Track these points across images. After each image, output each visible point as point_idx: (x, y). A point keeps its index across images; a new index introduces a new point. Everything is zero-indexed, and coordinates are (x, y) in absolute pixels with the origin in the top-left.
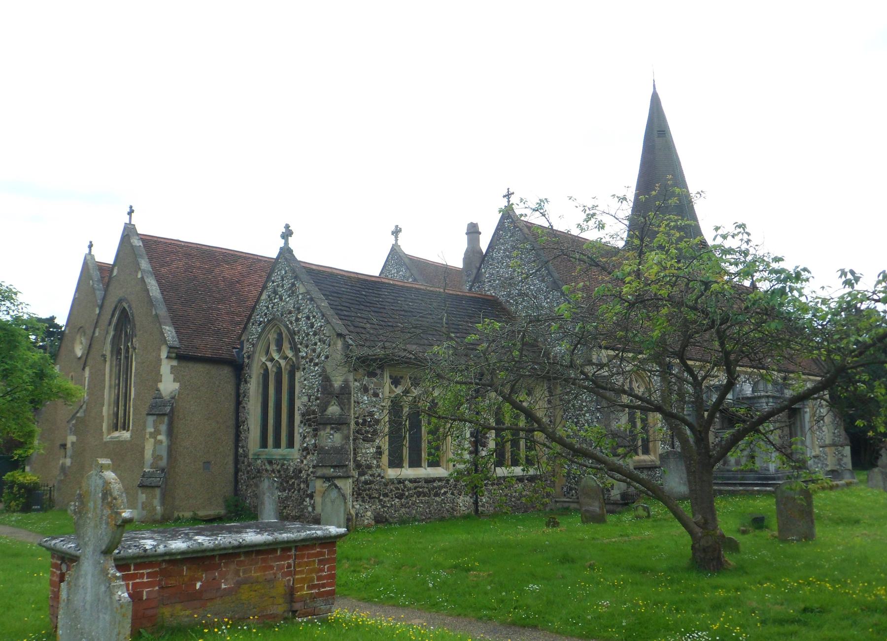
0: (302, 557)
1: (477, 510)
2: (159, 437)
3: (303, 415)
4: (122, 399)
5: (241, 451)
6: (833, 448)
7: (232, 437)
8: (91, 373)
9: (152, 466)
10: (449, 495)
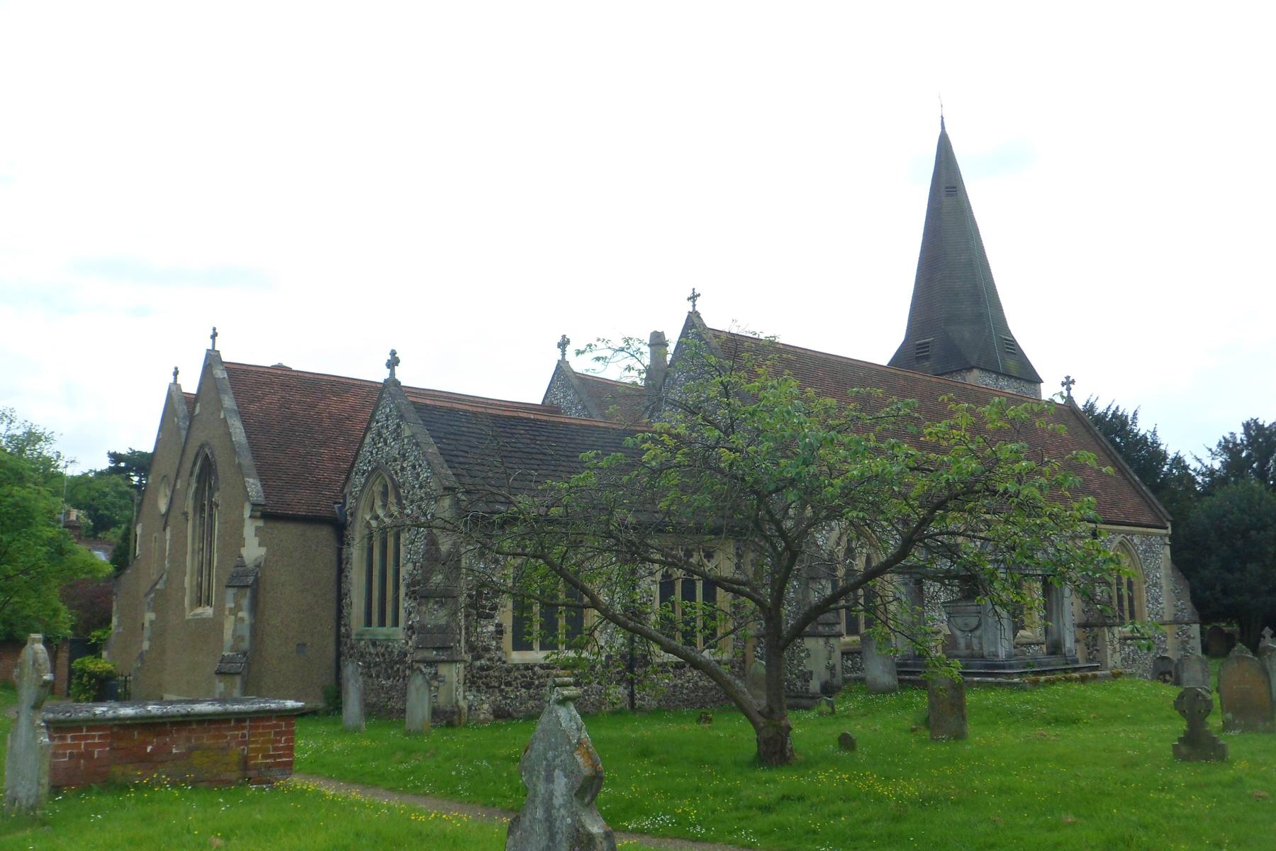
0: (258, 727)
1: (632, 705)
2: (240, 614)
3: (408, 586)
4: (204, 567)
5: (343, 630)
6: (1176, 627)
7: (333, 612)
8: (172, 536)
9: (232, 649)
10: (594, 685)
